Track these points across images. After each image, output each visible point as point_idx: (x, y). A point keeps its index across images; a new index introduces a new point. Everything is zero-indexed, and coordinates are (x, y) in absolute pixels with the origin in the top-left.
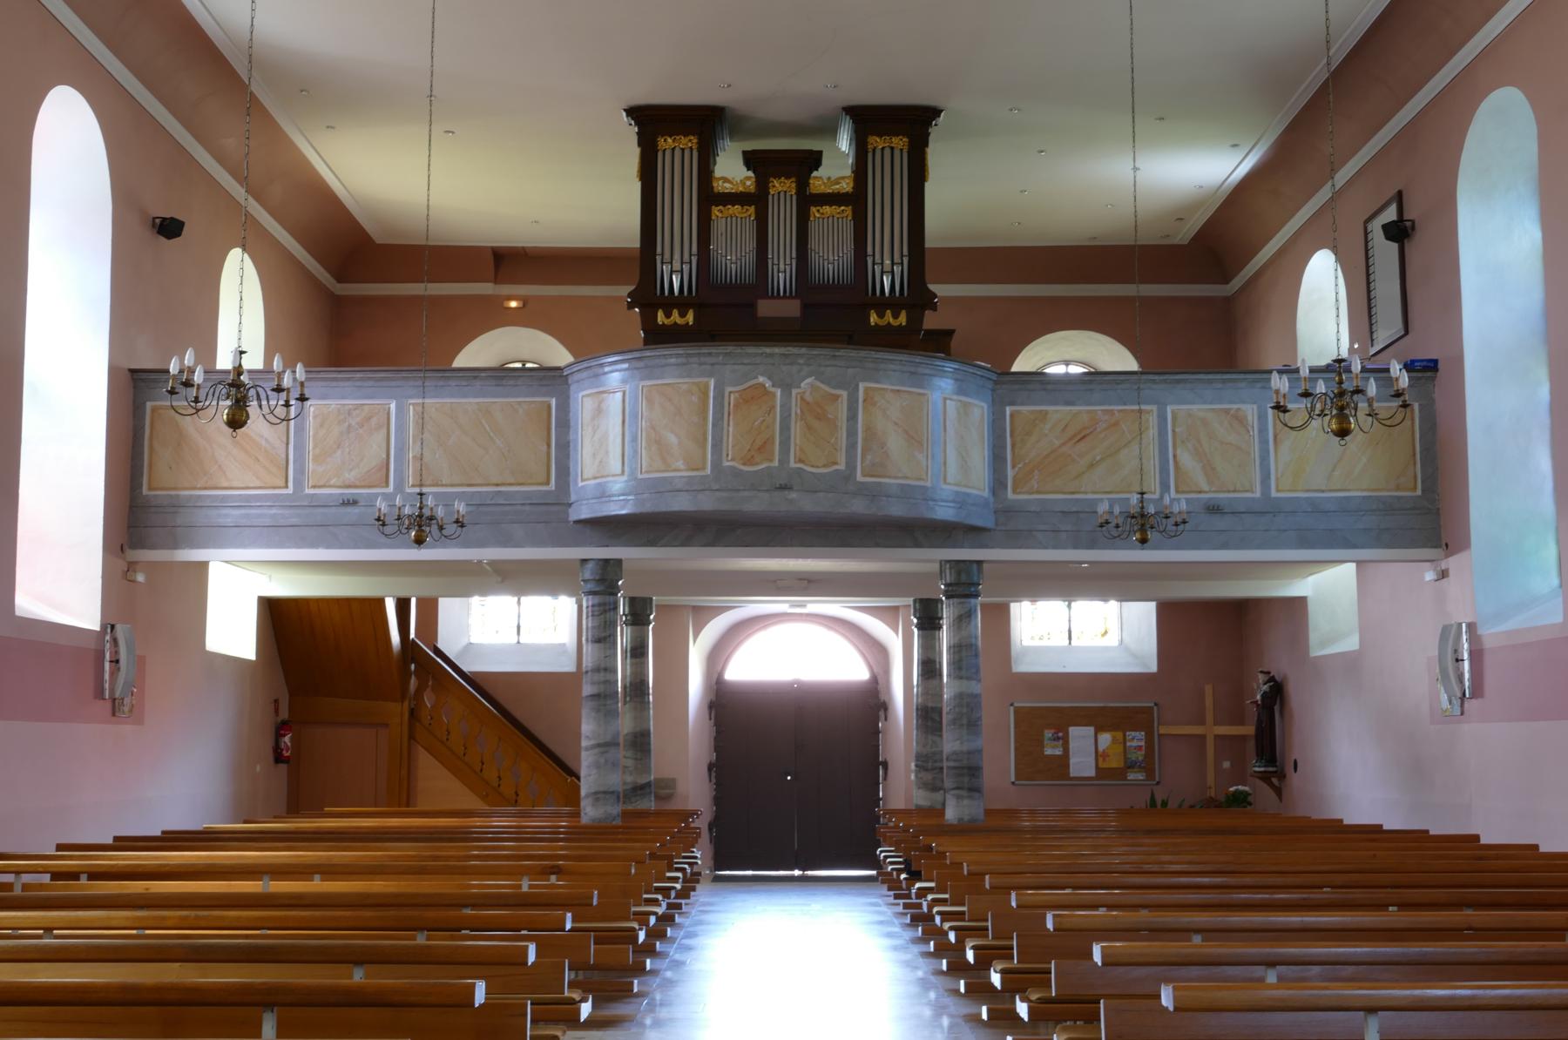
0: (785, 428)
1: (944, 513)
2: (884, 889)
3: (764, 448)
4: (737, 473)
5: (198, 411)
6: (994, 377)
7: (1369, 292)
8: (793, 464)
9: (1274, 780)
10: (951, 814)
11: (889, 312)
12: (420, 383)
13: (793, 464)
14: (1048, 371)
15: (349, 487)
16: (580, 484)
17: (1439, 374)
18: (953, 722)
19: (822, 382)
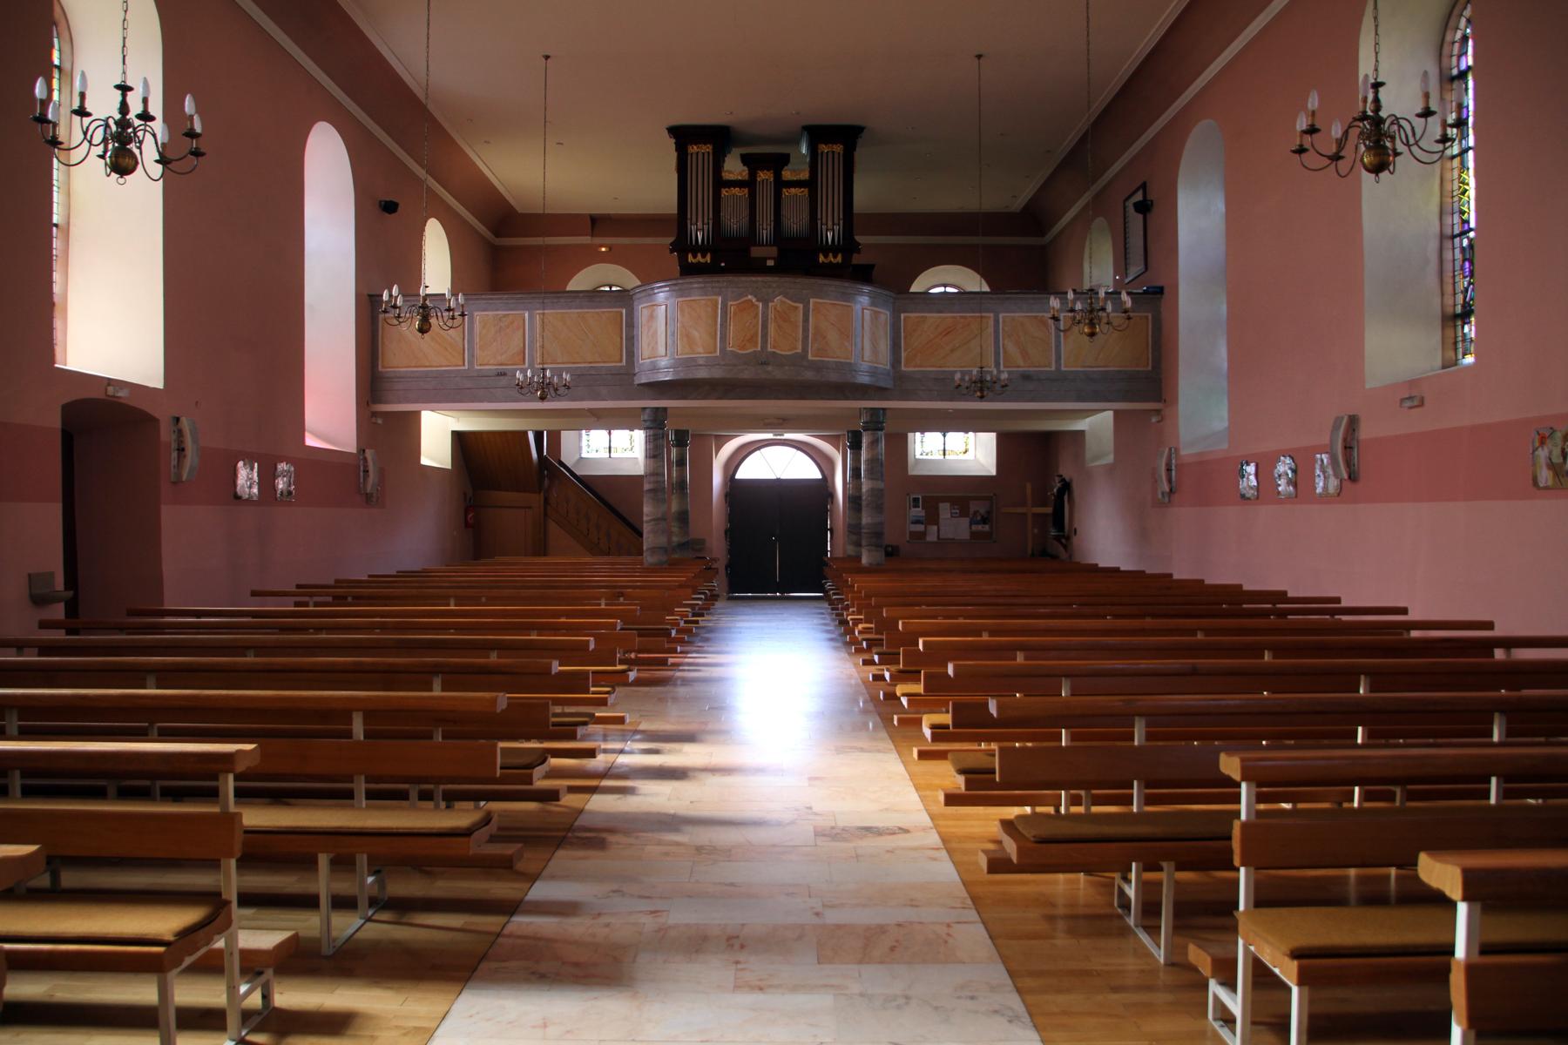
0: (765, 326)
1: (864, 379)
2: (826, 605)
3: (752, 340)
4: (734, 354)
5: (400, 322)
6: (894, 296)
7: (1125, 244)
8: (769, 350)
9: (1063, 541)
10: (865, 560)
11: (831, 255)
12: (541, 301)
13: (769, 350)
14: (931, 291)
15: (501, 365)
16: (641, 362)
17: (1164, 296)
18: (867, 505)
19: (787, 298)
